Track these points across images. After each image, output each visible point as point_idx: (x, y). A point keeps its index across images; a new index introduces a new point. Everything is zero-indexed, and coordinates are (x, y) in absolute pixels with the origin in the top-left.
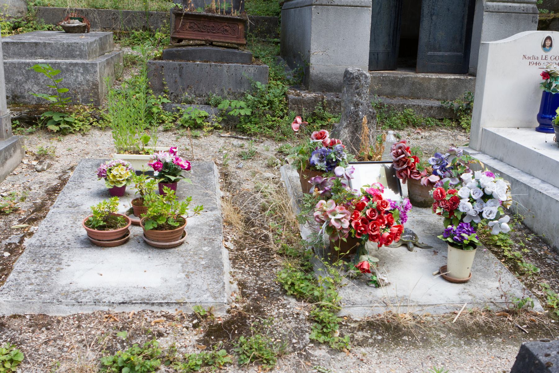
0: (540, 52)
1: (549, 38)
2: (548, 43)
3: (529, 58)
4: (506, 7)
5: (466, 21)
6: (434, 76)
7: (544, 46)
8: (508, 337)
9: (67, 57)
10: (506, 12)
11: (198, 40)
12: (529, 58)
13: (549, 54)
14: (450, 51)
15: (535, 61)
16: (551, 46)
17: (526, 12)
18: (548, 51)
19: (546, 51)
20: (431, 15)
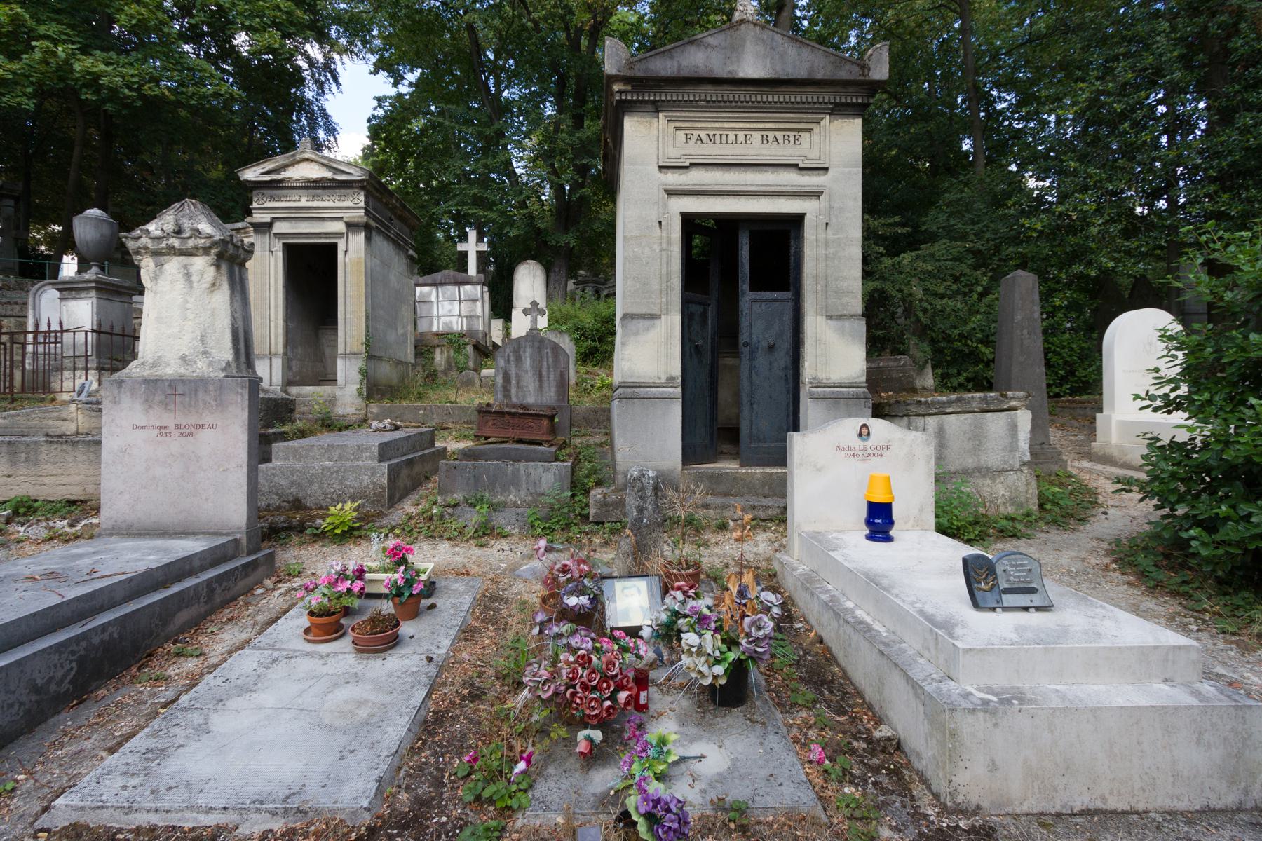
0: (857, 442)
1: (864, 426)
2: (865, 431)
3: (844, 449)
4: (833, 392)
5: (791, 409)
6: (759, 470)
7: (860, 435)
8: (503, 340)
9: (412, 459)
10: (104, 577)
11: (412, 427)
12: (844, 449)
13: (869, 443)
14: (777, 441)
15: (852, 452)
16: (869, 434)
17: (857, 397)
18: (867, 440)
19: (864, 440)
20: (751, 404)
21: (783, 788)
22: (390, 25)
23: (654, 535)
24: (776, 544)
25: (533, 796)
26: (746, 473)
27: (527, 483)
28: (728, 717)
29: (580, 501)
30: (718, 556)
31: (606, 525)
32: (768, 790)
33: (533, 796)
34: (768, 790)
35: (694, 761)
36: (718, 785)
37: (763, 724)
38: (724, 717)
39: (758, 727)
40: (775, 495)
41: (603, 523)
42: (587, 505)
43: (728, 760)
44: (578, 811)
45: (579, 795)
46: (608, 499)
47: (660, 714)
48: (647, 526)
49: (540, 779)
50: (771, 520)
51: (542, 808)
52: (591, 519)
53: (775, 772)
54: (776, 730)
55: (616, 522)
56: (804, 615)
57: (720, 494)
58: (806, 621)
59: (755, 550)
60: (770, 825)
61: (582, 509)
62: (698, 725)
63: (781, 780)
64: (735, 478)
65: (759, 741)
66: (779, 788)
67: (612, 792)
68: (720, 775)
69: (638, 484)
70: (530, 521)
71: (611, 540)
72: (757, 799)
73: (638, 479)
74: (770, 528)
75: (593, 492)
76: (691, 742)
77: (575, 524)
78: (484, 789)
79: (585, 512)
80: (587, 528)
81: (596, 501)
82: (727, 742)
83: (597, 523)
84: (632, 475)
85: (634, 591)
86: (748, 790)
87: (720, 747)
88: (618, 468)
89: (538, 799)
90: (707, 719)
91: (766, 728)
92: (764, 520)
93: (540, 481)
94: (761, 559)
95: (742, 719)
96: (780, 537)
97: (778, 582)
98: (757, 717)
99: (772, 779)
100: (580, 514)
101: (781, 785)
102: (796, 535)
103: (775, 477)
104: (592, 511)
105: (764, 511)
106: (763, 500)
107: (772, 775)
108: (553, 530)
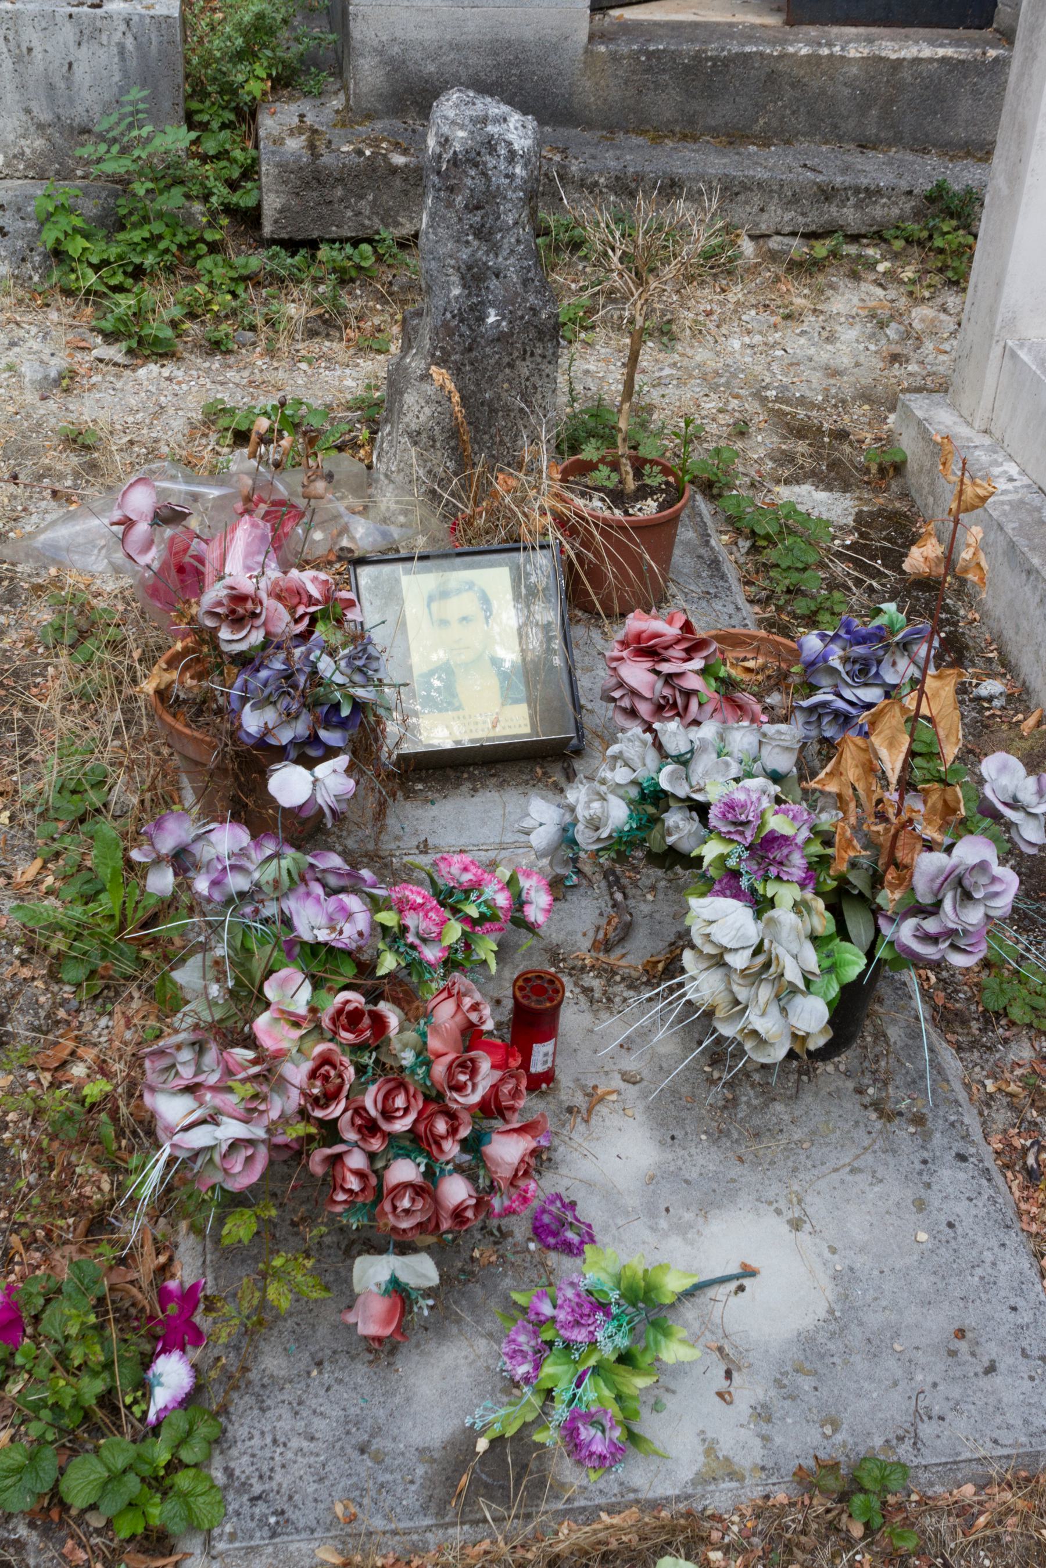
21: (997, 1380)
22: (722, 1071)
23: (524, 369)
24: (892, 331)
25: (229, 1472)
26: (814, 60)
27: (22, 87)
28: (808, 1098)
29: (222, 155)
30: (711, 381)
31: (324, 253)
32: (956, 1392)
33: (229, 1472)
34: (956, 1392)
35: (721, 1292)
36: (806, 1383)
37: (919, 1120)
38: (796, 1097)
39: (904, 1132)
40: (897, 140)
41: (313, 245)
42: (250, 172)
43: (825, 1281)
44: (378, 1523)
45: (378, 1459)
46: (327, 159)
47: (595, 1098)
48: (501, 338)
49: (241, 1402)
50: (879, 237)
51: (263, 1522)
52: (267, 229)
53: (970, 1321)
54: (958, 1146)
55: (356, 242)
56: (998, 639)
57: (714, 131)
58: (1006, 667)
59: (824, 355)
60: (965, 1512)
61: (233, 185)
62: (718, 1136)
63: (991, 1350)
64: (772, 78)
65: (909, 1194)
66: (984, 1382)
67: (482, 1445)
68: (806, 1341)
69: (471, 179)
70: (50, 236)
71: (342, 311)
72: (927, 1430)
73: (471, 159)
74: (872, 266)
75: (268, 124)
76: (705, 1209)
77: (214, 248)
78: (62, 1471)
79: (244, 200)
80: (255, 261)
81: (283, 167)
82: (816, 1206)
83: (291, 246)
84: (445, 142)
85: (465, 604)
86: (896, 1396)
87: (796, 1225)
88: (359, 30)
89: (245, 1486)
90: (742, 1111)
91: (927, 1136)
92: (854, 238)
93: (68, 79)
94: (848, 393)
95: (851, 1104)
96: (903, 302)
97: (905, 495)
98: (900, 1098)
99: (963, 1346)
100: (229, 210)
101: (991, 1369)
102: (997, 350)
103: (906, 75)
104: (272, 203)
105: (859, 206)
106: (858, 160)
107: (960, 1333)
108: (138, 273)
